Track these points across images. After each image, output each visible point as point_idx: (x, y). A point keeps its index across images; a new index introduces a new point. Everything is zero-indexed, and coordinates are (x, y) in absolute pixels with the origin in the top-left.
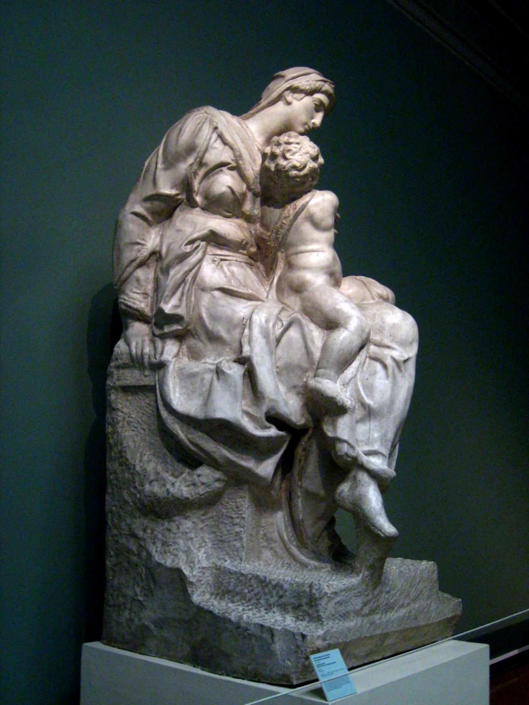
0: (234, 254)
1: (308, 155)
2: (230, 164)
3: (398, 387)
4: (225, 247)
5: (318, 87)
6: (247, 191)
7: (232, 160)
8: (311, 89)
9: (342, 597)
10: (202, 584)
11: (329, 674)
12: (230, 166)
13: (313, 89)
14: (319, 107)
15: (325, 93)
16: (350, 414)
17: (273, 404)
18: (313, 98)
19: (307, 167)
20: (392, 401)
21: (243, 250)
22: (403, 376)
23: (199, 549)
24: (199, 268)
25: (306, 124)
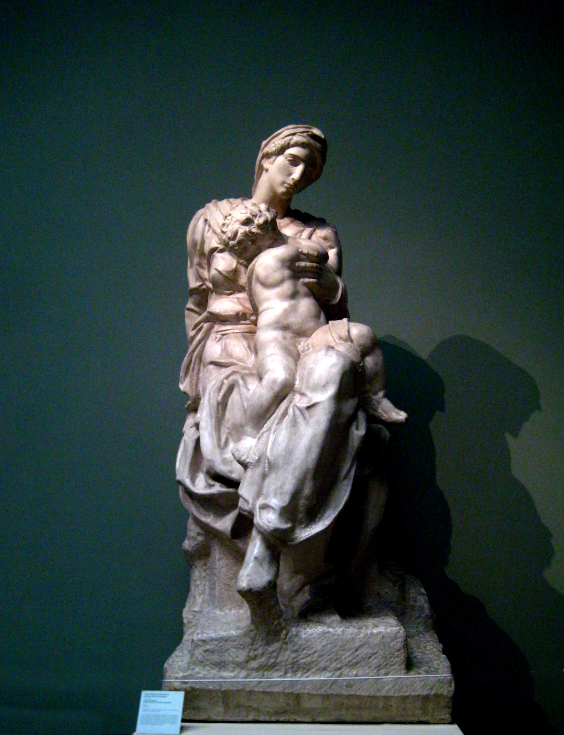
0: (236, 327)
1: (238, 222)
2: (217, 248)
3: (299, 436)
4: (228, 323)
5: (285, 144)
6: (239, 266)
7: (219, 244)
8: (278, 149)
9: (213, 646)
10: (193, 626)
11: (154, 710)
12: (219, 249)
13: (279, 148)
14: (294, 161)
15: (296, 145)
16: (252, 468)
17: (211, 464)
18: (284, 156)
19: (239, 234)
20: (289, 452)
21: (245, 320)
22: (307, 423)
23: (200, 595)
24: (204, 347)
25: (284, 183)
